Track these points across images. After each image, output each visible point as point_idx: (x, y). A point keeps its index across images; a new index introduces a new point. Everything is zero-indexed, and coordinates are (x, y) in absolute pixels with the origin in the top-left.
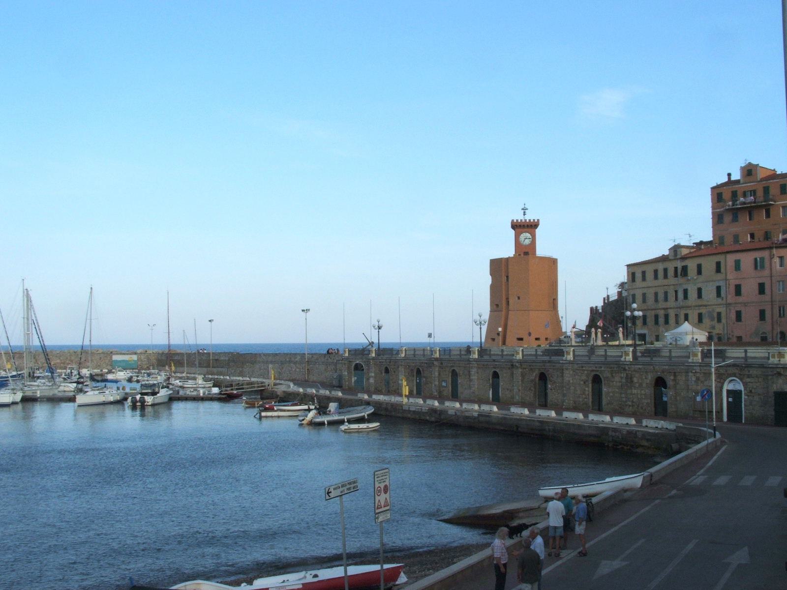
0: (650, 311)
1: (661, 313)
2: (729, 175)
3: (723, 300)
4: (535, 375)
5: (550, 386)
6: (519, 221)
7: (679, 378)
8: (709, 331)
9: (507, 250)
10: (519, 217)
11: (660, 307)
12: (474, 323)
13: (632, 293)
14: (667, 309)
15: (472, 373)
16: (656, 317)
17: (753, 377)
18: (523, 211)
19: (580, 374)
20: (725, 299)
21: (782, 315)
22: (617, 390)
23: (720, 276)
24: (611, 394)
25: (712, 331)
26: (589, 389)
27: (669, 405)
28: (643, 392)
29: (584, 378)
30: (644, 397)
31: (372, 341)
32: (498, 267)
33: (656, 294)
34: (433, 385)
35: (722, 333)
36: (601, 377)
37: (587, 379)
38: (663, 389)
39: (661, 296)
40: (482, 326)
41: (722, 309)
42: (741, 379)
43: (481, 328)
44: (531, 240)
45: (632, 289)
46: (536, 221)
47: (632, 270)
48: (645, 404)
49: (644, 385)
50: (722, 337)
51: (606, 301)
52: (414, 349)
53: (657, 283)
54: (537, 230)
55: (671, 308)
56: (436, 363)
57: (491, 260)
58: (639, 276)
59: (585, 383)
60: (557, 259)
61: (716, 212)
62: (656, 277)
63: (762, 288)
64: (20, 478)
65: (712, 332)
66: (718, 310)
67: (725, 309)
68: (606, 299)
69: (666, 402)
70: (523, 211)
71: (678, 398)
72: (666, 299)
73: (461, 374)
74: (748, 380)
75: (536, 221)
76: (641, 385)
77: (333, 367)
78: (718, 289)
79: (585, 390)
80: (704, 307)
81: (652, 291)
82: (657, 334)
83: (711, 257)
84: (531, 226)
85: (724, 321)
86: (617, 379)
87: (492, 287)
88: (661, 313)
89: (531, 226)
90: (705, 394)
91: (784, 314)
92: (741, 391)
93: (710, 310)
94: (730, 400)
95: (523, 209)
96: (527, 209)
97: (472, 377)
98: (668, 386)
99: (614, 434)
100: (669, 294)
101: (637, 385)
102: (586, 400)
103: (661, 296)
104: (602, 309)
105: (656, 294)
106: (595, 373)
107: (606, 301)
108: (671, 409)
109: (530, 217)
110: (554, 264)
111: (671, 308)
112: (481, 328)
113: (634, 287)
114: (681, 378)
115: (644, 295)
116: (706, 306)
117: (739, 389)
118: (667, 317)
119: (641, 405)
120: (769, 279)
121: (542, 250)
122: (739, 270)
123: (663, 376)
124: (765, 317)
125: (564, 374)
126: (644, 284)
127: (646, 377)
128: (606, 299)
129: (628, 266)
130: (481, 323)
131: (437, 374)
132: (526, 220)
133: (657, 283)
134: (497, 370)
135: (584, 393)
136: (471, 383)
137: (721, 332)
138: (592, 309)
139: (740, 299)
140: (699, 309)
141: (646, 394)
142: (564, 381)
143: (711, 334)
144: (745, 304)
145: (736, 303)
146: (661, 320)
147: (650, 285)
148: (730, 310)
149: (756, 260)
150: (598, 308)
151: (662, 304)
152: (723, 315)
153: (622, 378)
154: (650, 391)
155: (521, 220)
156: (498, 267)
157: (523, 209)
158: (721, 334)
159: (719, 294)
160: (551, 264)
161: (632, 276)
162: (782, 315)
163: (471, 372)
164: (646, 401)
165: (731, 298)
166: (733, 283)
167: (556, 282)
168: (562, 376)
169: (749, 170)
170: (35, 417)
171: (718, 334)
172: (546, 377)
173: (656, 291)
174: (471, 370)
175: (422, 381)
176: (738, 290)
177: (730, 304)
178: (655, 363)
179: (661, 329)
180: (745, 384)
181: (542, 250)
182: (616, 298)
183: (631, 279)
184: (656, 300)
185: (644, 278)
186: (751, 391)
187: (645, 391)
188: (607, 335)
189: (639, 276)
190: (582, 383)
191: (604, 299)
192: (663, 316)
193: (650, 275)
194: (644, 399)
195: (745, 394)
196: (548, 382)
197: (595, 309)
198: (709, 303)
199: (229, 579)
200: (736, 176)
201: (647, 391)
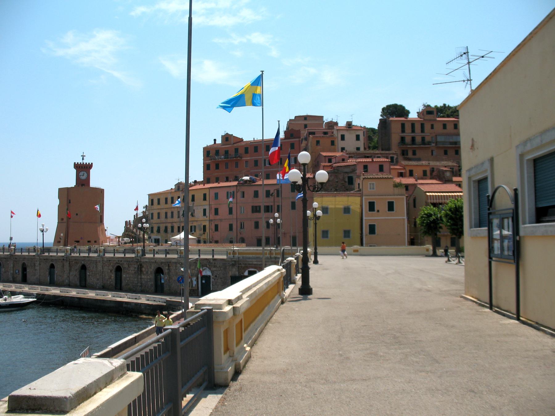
0: (162, 224)
1: (169, 226)
2: (215, 140)
3: (207, 217)
4: (48, 265)
5: (88, 273)
6: (79, 163)
7: (171, 267)
8: (199, 237)
9: (71, 182)
10: (80, 161)
11: (168, 222)
13: (151, 212)
14: (173, 222)
15: (37, 265)
16: (166, 228)
17: (218, 267)
18: (82, 157)
19: (108, 265)
20: (208, 217)
21: (243, 227)
22: (132, 276)
23: (207, 202)
24: (128, 279)
25: (200, 237)
26: (113, 276)
27: (165, 285)
28: (148, 277)
29: (111, 268)
30: (149, 281)
32: (64, 193)
33: (166, 213)
34: (10, 273)
35: (207, 238)
36: (122, 267)
37: (113, 269)
38: (161, 275)
39: (169, 215)
41: (207, 224)
42: (210, 269)
43: (43, 234)
44: (80, 174)
45: (152, 210)
46: (90, 164)
47: (151, 198)
48: (150, 285)
49: (149, 273)
50: (206, 241)
51: (136, 217)
52: (29, 249)
53: (167, 206)
54: (91, 171)
55: (175, 222)
58: (156, 202)
59: (111, 271)
60: (103, 190)
61: (206, 163)
62: (166, 203)
63: (231, 211)
64: (414, 344)
65: (200, 238)
66: (204, 224)
67: (208, 223)
68: (136, 216)
69: (163, 283)
71: (171, 281)
72: (172, 217)
73: (29, 266)
74: (214, 269)
75: (90, 164)
76: (147, 273)
78: (205, 210)
79: (111, 276)
80: (196, 222)
81: (164, 211)
82: (166, 239)
83: (507, 224)
84: (88, 167)
85: (207, 230)
86: (132, 268)
87: (59, 207)
88: (169, 226)
89: (88, 167)
90: (181, 280)
91: (244, 227)
92: (210, 276)
93: (200, 223)
94: (204, 281)
96: (85, 156)
97: (36, 268)
98: (164, 273)
99: (126, 305)
100: (174, 214)
101: (145, 273)
102: (112, 282)
103: (169, 215)
105: (166, 213)
106: (117, 265)
107: (136, 217)
108: (166, 289)
109: (87, 161)
110: (101, 192)
111: (175, 222)
112: (43, 234)
113: (152, 208)
114: (173, 268)
115: (159, 214)
116: (197, 221)
117: (209, 275)
118: (172, 228)
119: (147, 286)
120: (236, 205)
121: (93, 184)
122: (217, 199)
123: (161, 266)
124: (215, 227)
125: (98, 266)
126: (159, 207)
127: (150, 267)
128: (136, 216)
129: (149, 195)
131: (12, 265)
132: (83, 163)
133: (167, 206)
134: (54, 263)
135: (110, 278)
136: (36, 272)
137: (205, 238)
138: (126, 222)
139: (218, 217)
140: (197, 223)
141: (150, 278)
142: (98, 270)
143: (200, 239)
144: (221, 220)
145: (215, 220)
146: (169, 230)
147: (163, 207)
148: (211, 224)
149: (228, 193)
150: (131, 222)
151: (169, 220)
152: (207, 227)
153: (135, 268)
154: (152, 277)
155: (80, 163)
156: (64, 193)
157: (82, 156)
158: (206, 239)
159: (205, 214)
160: (100, 193)
161: (152, 202)
162: (243, 227)
163: (36, 264)
164: (150, 283)
165: (213, 216)
166: (214, 207)
167: (102, 205)
168: (96, 267)
169: (227, 138)
171: (204, 239)
172: (86, 268)
173: (166, 211)
174: (36, 263)
175: (2, 270)
176: (216, 212)
177: (211, 220)
179: (169, 235)
180: (212, 272)
181: (93, 184)
182: (142, 215)
183: (151, 203)
184: (166, 217)
185: (159, 203)
186: (216, 276)
187: (150, 277)
188: (133, 240)
189: (156, 202)
190: (109, 271)
191: (134, 216)
192: (177, 228)
193: (163, 201)
194: (149, 282)
195: (212, 278)
196: (87, 271)
197: (128, 222)
198: (199, 220)
200: (219, 141)
201: (151, 276)
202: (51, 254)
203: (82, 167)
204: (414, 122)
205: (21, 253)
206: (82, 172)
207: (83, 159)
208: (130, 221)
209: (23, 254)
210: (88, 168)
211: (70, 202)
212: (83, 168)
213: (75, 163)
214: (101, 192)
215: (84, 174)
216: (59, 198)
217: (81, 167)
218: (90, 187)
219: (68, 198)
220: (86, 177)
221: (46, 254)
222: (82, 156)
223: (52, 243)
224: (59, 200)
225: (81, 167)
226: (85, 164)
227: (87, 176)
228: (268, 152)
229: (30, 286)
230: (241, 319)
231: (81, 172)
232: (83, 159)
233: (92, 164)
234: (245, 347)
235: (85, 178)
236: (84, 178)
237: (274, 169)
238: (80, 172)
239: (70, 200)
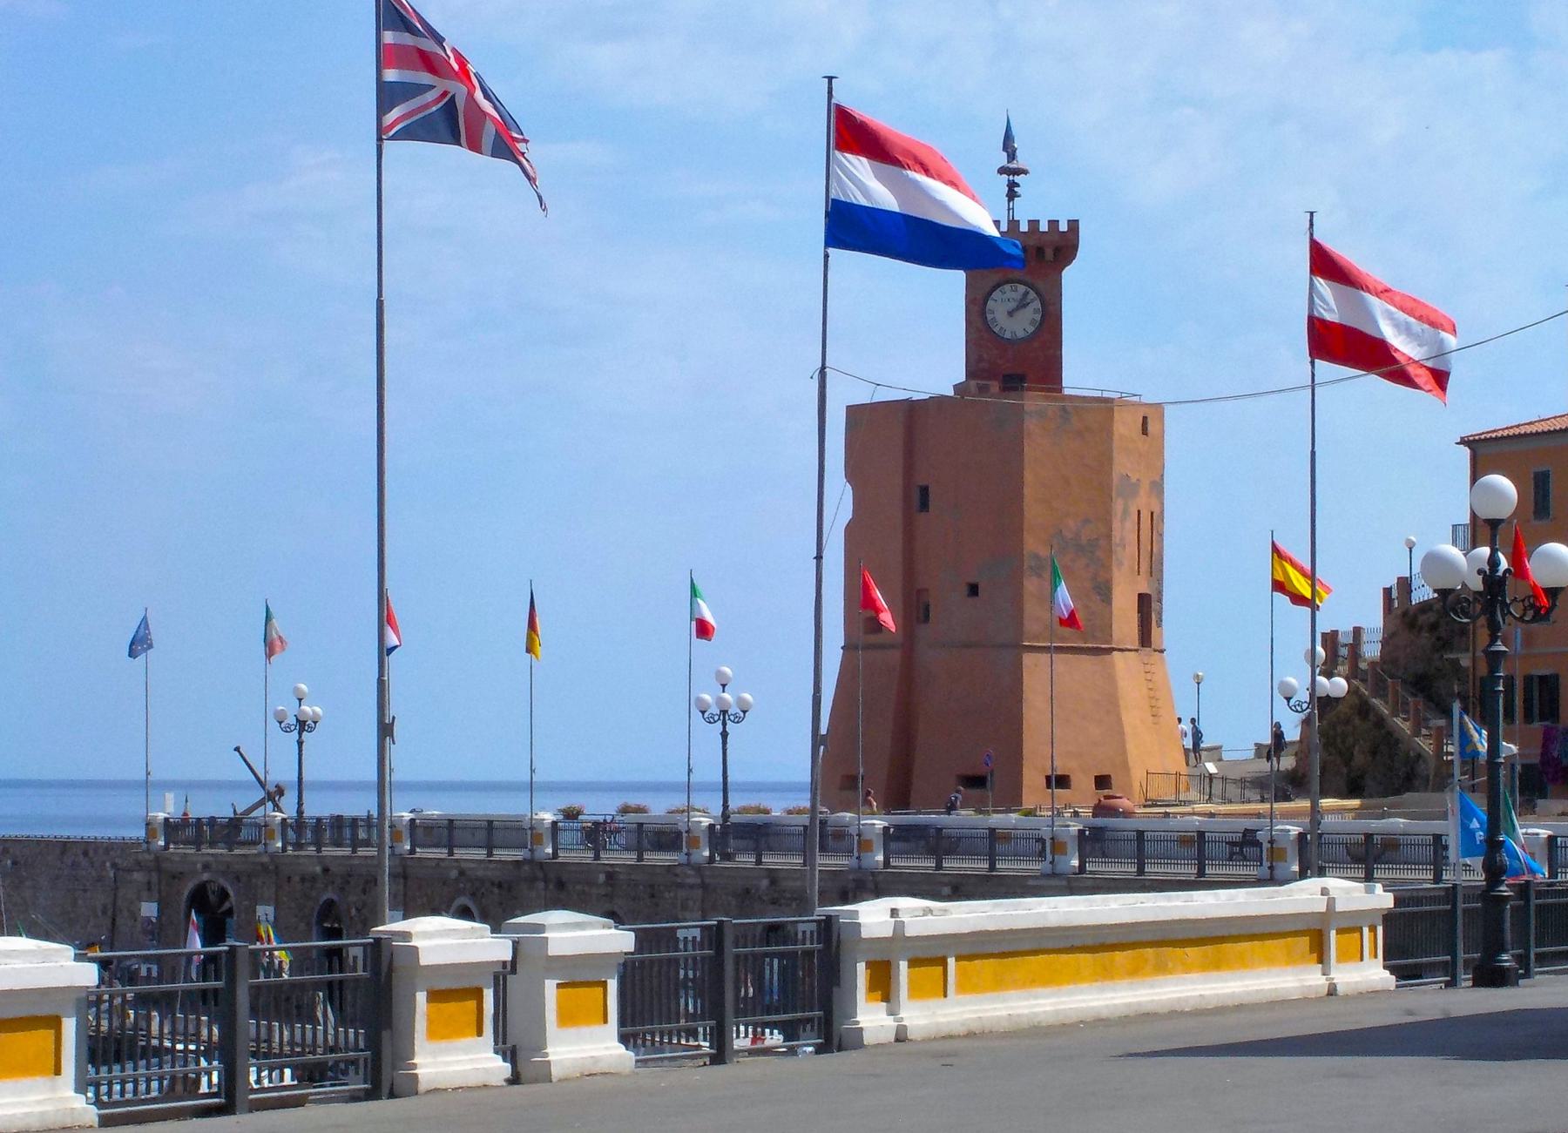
12: (696, 714)
31: (529, 655)
40: (730, 725)
43: (724, 735)
46: (1063, 227)
54: (1071, 276)
56: (360, 823)
57: (848, 407)
68: (1395, 594)
70: (1020, 161)
75: (1063, 227)
77: (101, 899)
95: (1002, 171)
96: (1025, 172)
104: (1385, 642)
110: (1145, 431)
112: (724, 735)
130: (724, 712)
157: (1002, 171)
170: (1464, 585)
178: (1418, 855)
191: (1387, 592)
199: (183, 933)
202: (771, 861)
205: (445, 851)
206: (1007, 287)
208: (1357, 631)
209: (460, 853)
210: (1049, 254)
211: (924, 505)
214: (1145, 431)
218: (1067, 392)
219: (909, 469)
220: (1033, 322)
221: (746, 860)
227: (1008, 335)
230: (284, 811)
231: (998, 286)
233: (1074, 225)
234: (901, 1037)
236: (1017, 325)
239: (925, 491)
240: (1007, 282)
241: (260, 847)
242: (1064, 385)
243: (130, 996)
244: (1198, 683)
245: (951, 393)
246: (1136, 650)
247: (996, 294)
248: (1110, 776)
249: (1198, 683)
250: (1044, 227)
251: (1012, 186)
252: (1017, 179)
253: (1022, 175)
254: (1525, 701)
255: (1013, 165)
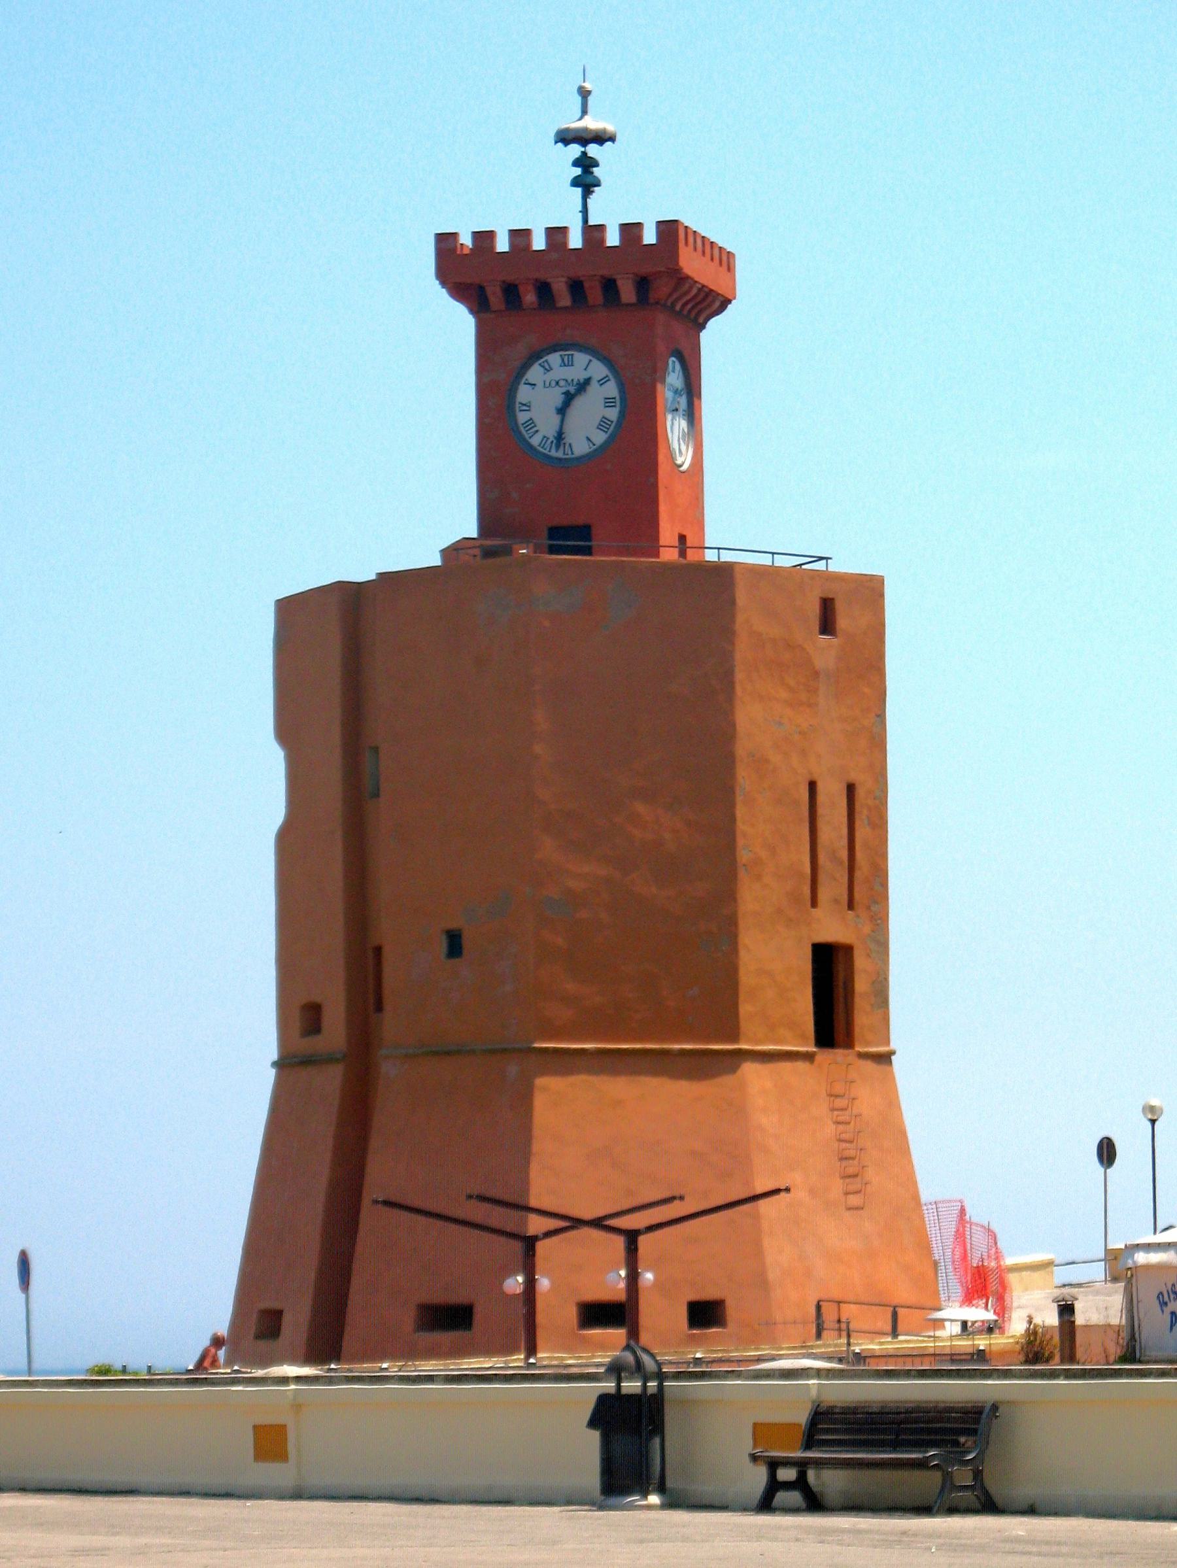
18: (575, 150)
46: (650, 237)
132: (593, 233)
157: (565, 138)
203: (544, 289)
204: (263, 1345)
206: (554, 359)
207: (586, 183)
212: (627, 292)
213: (445, 242)
215: (583, 386)
216: (382, 576)
217: (530, 297)
220: (603, 424)
222: (565, 138)
223: (795, 1425)
224: (373, 577)
225: (530, 297)
226: (613, 239)
227: (613, 414)
228: (737, 569)
229: (431, 1362)
231: (535, 356)
232: (586, 183)
235: (600, 438)
237: (865, 1437)
238: (526, 367)
240: (554, 349)
241: (848, 1112)
242: (662, 543)
243: (991, 1252)
244: (1153, 1122)
245: (436, 561)
246: (809, 1057)
247: (535, 373)
248: (470, 1330)
249: (1153, 1122)
250: (539, 243)
251: (586, 164)
252: (593, 150)
253: (609, 143)
254: (814, 1359)
255: (591, 123)
